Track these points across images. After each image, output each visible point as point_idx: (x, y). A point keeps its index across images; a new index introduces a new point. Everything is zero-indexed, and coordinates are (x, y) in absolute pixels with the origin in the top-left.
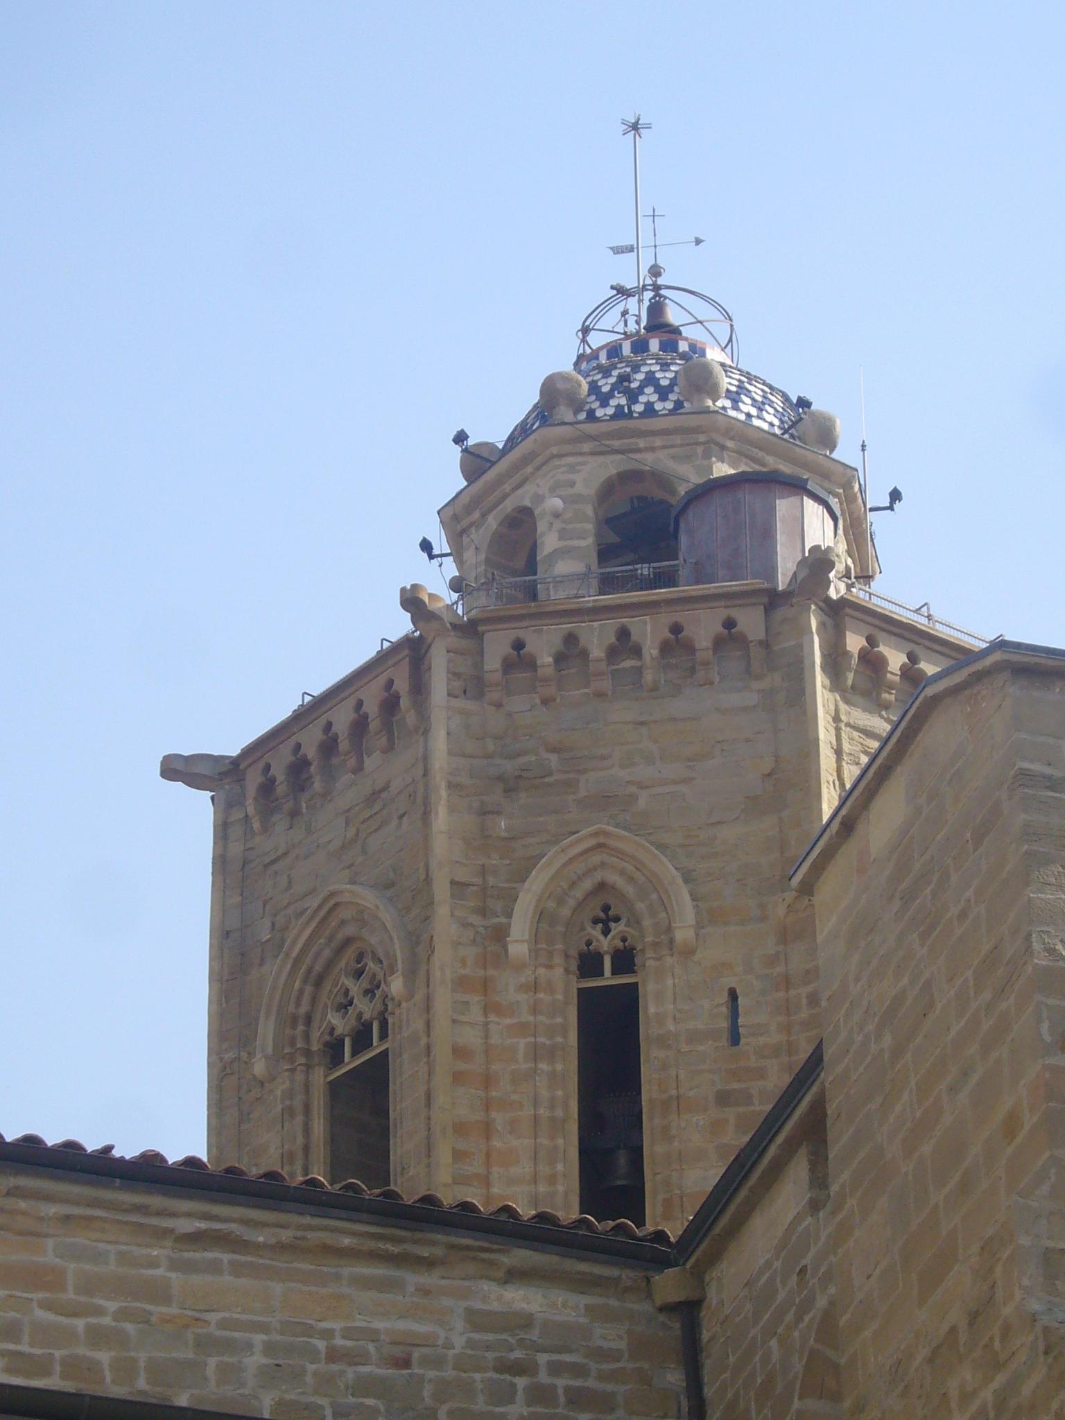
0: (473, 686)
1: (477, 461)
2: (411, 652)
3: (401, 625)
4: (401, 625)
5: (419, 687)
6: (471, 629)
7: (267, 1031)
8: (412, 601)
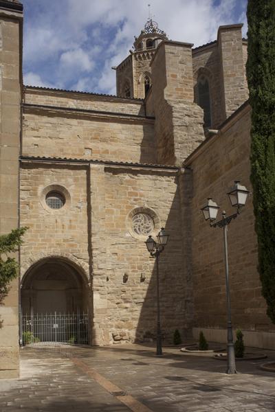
0: (136, 59)
1: (136, 39)
2: (131, 56)
3: (130, 54)
4: (130, 54)
5: (132, 59)
6: (136, 54)
7: (121, 90)
8: (130, 51)
